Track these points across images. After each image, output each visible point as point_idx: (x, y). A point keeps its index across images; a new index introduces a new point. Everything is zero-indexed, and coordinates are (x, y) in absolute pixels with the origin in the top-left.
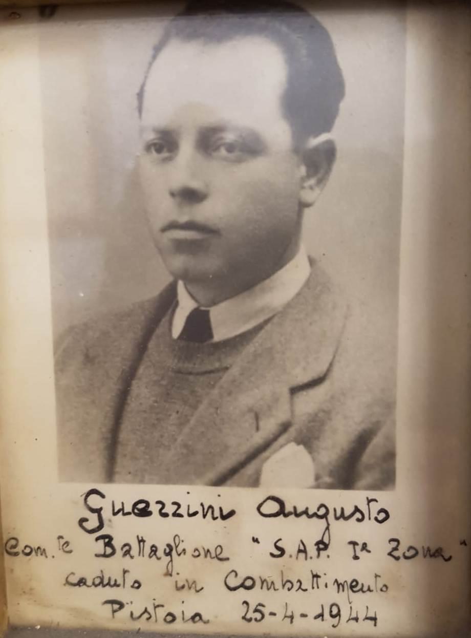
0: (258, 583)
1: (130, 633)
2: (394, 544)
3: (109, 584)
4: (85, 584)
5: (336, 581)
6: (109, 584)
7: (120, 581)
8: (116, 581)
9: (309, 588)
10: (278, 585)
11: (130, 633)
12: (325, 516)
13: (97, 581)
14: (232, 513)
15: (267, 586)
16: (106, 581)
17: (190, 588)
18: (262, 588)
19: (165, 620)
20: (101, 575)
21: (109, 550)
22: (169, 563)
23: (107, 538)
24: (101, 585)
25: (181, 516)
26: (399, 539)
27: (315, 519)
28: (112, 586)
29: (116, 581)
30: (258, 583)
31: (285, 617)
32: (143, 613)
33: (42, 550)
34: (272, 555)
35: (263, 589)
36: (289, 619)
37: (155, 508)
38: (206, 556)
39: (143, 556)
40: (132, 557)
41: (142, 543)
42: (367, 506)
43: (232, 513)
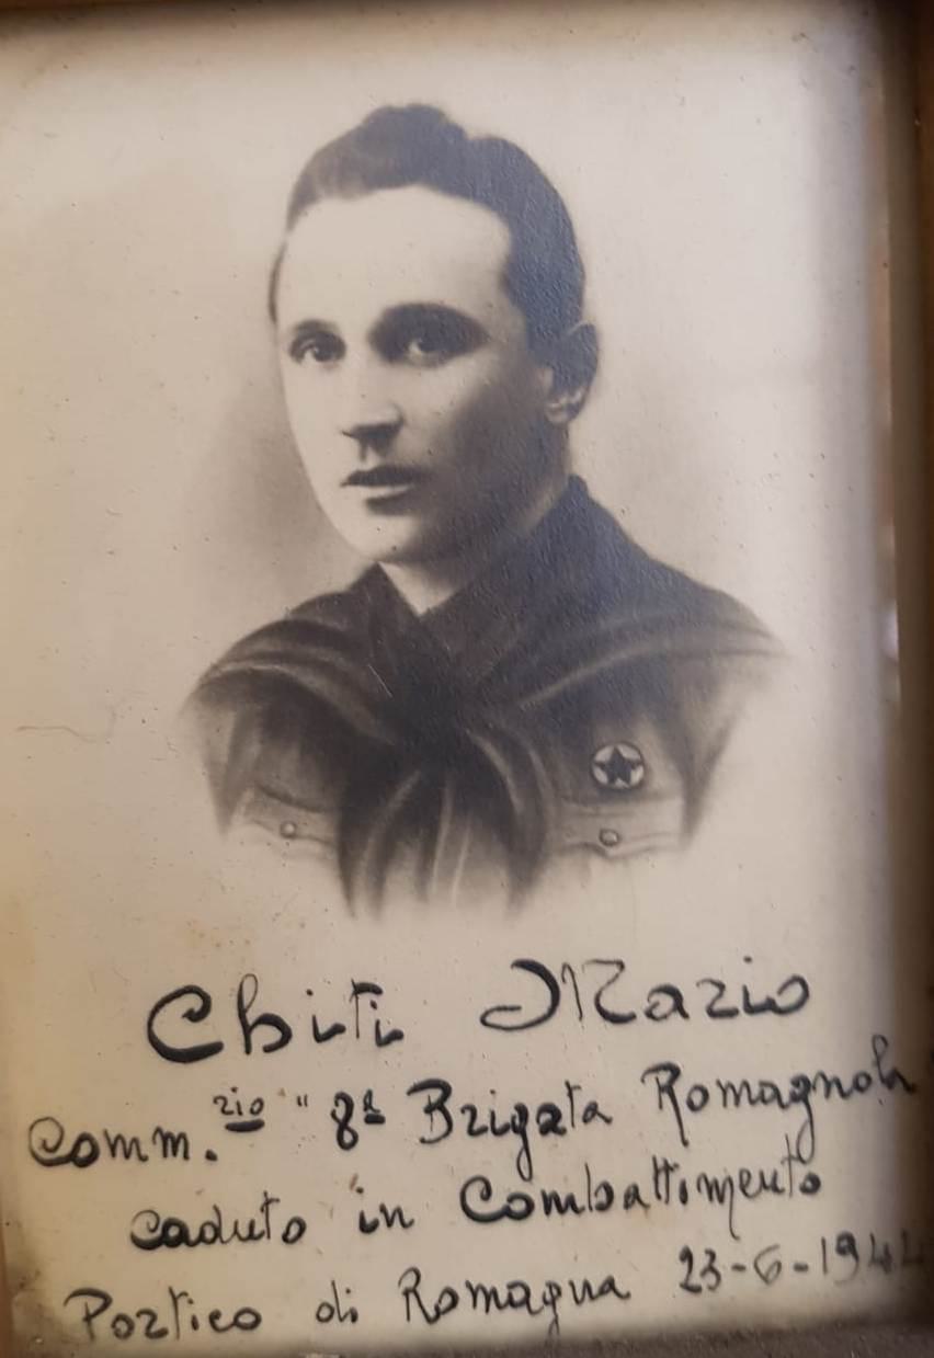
1: (840, 1325)
2: (221, 1102)
3: (201, 1238)
4: (183, 1238)
6: (201, 1238)
7: (783, 1183)
8: (775, 1178)
10: (581, 1202)
11: (840, 1325)
12: (521, 1131)
14: (396, 1036)
16: (227, 1232)
17: (390, 1223)
18: (725, 1104)
19: (117, 1334)
20: (216, 1221)
22: (520, 1154)
23: (521, 1119)
24: (218, 1241)
25: (731, 1013)
27: (769, 1018)
28: (192, 1244)
29: (252, 1226)
31: (657, 1172)
34: (269, 1237)
35: (247, 1222)
36: (177, 1293)
37: (695, 1001)
38: (548, 1211)
39: (186, 1157)
40: (143, 1159)
41: (662, 1178)
42: (568, 1099)
43: (396, 1036)
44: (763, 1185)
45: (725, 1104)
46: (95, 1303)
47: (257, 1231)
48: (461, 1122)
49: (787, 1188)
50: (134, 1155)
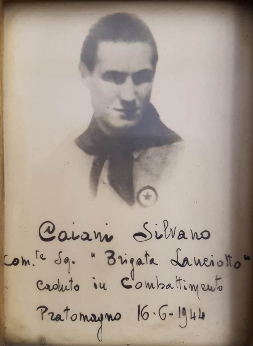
0: (144, 285)
5: (190, 285)
9: (146, 263)
10: (155, 285)
13: (56, 287)
15: (149, 285)
18: (81, 320)
21: (111, 261)
24: (61, 291)
26: (79, 291)
28: (210, 290)
30: (144, 285)
32: (227, 259)
33: (192, 285)
34: (29, 264)
44: (208, 289)
45: (81, 320)
46: (44, 309)
47: (68, 288)
48: (118, 261)
49: (70, 288)
50: (150, 285)
